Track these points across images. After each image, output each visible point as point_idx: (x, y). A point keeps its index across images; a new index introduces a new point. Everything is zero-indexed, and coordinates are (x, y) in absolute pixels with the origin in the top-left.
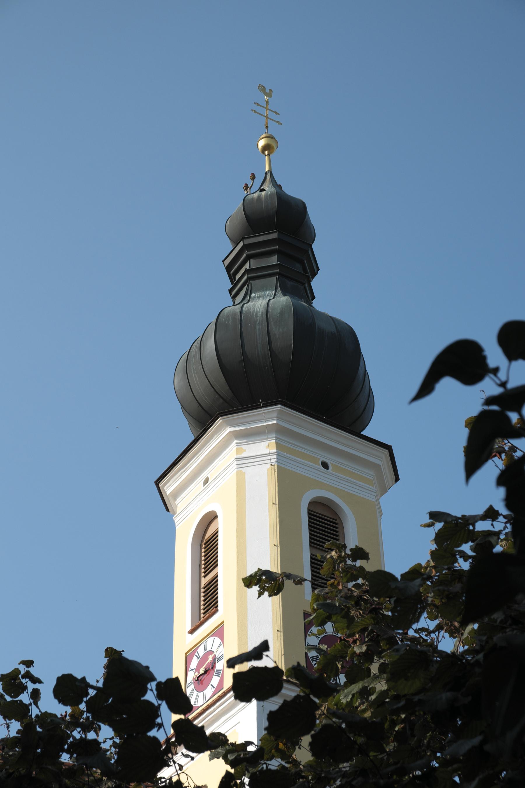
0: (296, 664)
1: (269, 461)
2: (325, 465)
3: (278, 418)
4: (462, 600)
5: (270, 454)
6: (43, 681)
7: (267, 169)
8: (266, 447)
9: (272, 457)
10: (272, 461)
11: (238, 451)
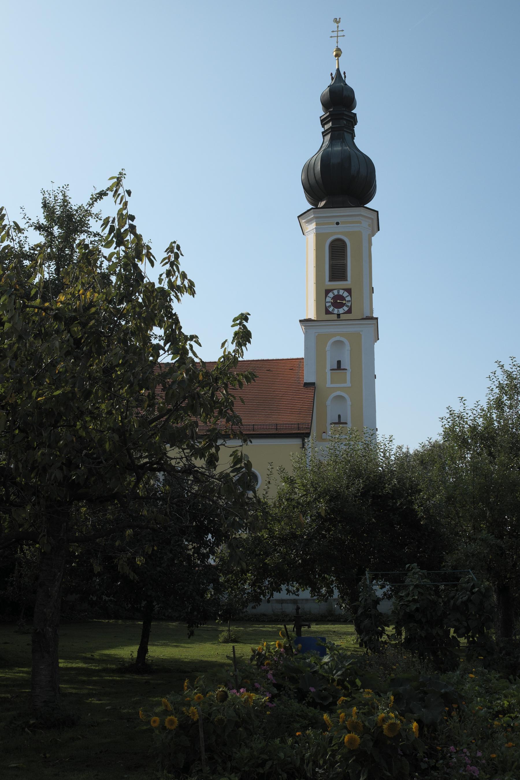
3: (314, 214)
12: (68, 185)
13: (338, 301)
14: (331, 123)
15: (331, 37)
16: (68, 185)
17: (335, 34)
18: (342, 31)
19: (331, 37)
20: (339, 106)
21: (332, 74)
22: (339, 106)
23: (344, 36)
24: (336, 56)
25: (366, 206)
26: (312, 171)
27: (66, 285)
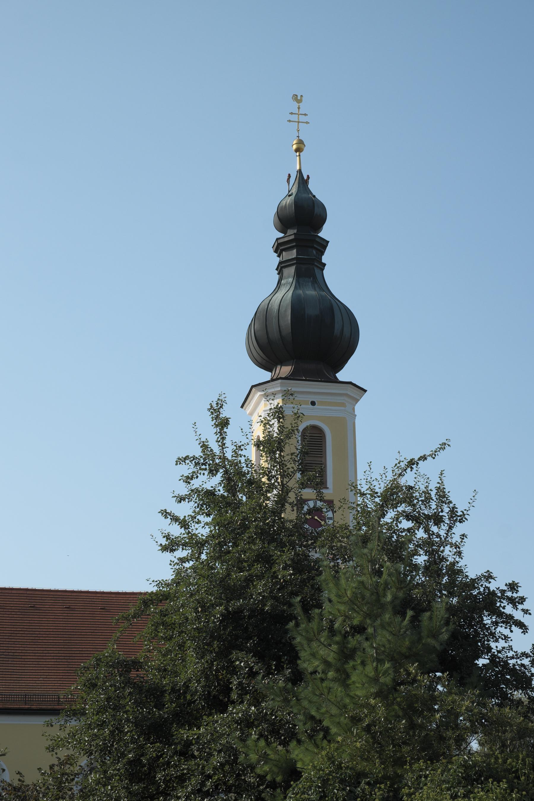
0: (516, 582)
2: (313, 403)
3: (281, 386)
6: (280, 193)
7: (298, 168)
12: (371, 462)
13: (316, 518)
15: (289, 121)
16: (371, 462)
17: (294, 118)
18: (305, 115)
19: (289, 121)
20: (302, 227)
22: (302, 227)
24: (297, 150)
25: (341, 376)
26: (275, 321)
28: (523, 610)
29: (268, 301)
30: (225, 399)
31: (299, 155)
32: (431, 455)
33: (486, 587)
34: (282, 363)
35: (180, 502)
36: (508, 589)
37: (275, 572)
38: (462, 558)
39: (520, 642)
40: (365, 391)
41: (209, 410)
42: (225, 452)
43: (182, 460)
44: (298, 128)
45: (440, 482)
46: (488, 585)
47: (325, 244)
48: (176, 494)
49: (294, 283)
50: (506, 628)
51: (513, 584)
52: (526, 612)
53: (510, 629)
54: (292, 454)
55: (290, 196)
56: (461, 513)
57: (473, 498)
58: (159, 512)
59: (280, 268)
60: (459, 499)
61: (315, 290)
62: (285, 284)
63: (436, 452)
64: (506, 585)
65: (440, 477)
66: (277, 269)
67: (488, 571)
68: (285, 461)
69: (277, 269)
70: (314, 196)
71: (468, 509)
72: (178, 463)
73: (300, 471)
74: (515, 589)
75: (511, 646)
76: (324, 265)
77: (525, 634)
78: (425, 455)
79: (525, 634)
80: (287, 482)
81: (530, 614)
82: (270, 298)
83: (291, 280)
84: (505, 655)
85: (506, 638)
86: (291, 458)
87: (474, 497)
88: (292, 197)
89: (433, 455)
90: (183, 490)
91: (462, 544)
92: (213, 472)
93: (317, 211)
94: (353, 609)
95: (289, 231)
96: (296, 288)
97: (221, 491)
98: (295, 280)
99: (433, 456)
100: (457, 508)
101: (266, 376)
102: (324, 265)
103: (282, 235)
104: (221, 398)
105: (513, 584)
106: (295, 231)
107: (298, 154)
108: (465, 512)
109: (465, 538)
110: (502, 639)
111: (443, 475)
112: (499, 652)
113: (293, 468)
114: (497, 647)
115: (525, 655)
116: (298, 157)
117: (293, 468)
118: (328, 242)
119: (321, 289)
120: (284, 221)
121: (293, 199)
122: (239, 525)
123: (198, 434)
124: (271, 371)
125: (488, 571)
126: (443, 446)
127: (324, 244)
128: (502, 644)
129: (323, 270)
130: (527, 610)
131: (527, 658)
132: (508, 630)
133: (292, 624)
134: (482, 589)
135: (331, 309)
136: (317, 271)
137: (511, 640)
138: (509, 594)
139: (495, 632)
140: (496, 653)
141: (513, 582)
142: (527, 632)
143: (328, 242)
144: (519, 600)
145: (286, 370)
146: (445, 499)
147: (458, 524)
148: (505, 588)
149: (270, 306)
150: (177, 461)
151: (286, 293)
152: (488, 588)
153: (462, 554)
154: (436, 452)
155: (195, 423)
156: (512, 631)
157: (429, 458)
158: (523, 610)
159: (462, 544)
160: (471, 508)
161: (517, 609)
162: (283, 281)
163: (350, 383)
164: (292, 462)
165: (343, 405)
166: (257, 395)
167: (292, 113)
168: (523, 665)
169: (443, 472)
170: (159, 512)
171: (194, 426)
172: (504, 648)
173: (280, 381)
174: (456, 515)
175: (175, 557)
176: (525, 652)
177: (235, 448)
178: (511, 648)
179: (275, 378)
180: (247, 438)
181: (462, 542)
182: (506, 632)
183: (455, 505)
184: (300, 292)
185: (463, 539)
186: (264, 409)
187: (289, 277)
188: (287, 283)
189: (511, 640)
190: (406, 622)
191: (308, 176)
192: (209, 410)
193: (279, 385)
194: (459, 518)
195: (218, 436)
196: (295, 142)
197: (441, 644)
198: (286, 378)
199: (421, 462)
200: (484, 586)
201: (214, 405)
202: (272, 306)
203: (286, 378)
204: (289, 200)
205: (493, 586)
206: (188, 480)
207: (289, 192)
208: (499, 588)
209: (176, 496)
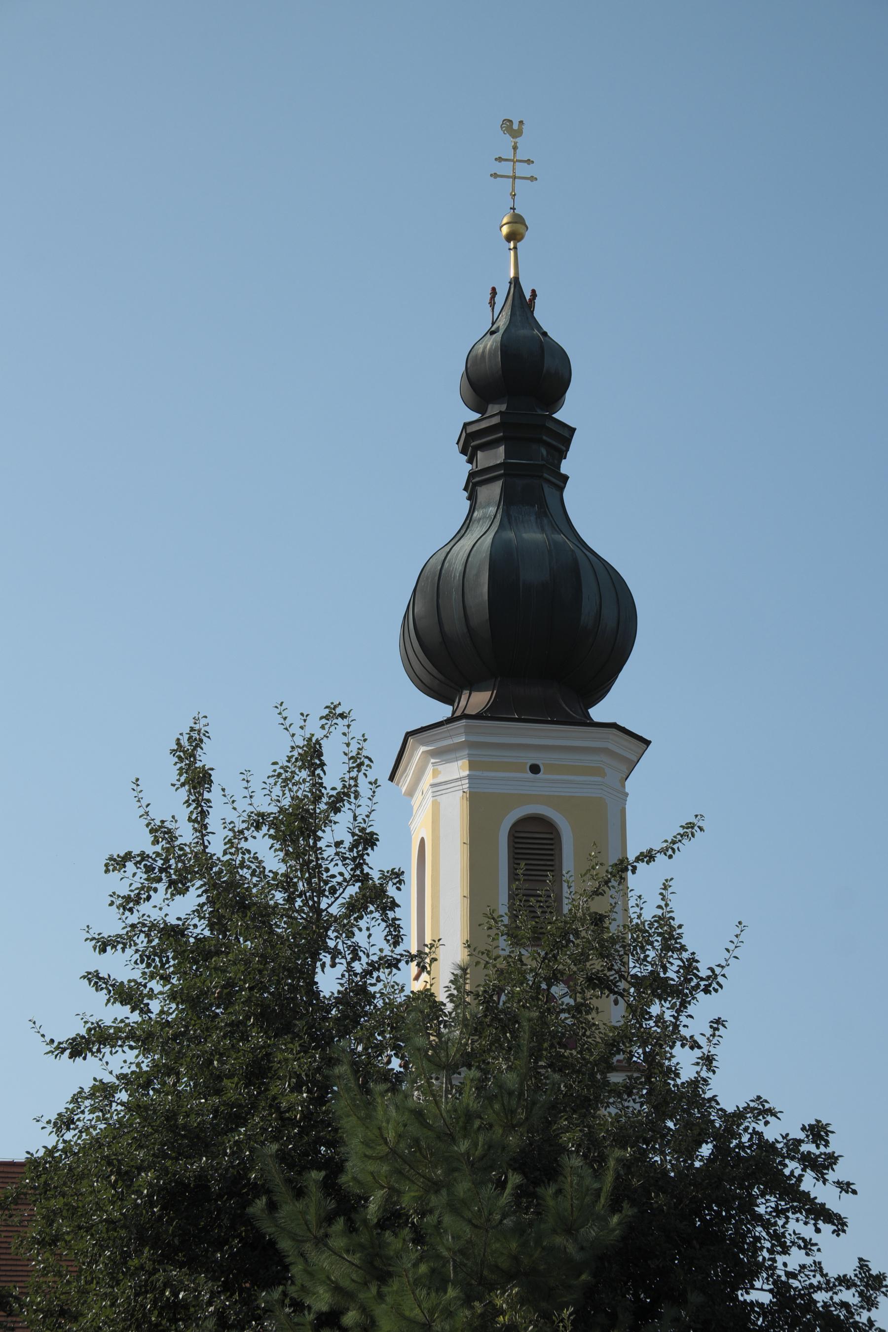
0: (824, 1123)
1: (461, 787)
2: (535, 769)
3: (467, 733)
4: (677, 1259)
5: (460, 779)
6: (472, 327)
7: (512, 275)
8: (457, 769)
9: (463, 782)
10: (464, 787)
11: (435, 773)
14: (502, 449)
15: (495, 175)
17: (506, 168)
18: (529, 162)
19: (495, 175)
20: (519, 398)
21: (494, 292)
22: (519, 398)
23: (532, 179)
24: (510, 237)
25: (598, 713)
26: (456, 596)
27: (262, 1059)
28: (838, 1184)
29: (444, 555)
30: (206, 728)
31: (515, 248)
32: (664, 851)
33: (755, 1132)
34: (473, 685)
35: (104, 951)
36: (807, 1136)
37: (274, 1098)
38: (714, 1072)
39: (837, 1255)
40: (647, 743)
41: (173, 752)
42: (206, 843)
43: (118, 863)
44: (513, 190)
45: (663, 904)
46: (760, 1127)
47: (566, 434)
48: (94, 933)
49: (499, 516)
50: (806, 1223)
51: (818, 1126)
52: (845, 1187)
53: (815, 1225)
54: (338, 844)
55: (492, 333)
56: (710, 973)
57: (735, 940)
58: (84, 977)
59: (472, 486)
60: (703, 943)
61: (543, 530)
62: (480, 519)
63: (674, 842)
64: (803, 1129)
65: (661, 894)
66: (465, 489)
67: (759, 1098)
68: (323, 858)
69: (465, 489)
70: (545, 334)
71: (724, 963)
72: (111, 868)
73: (357, 881)
74: (822, 1138)
75: (820, 1263)
76: (565, 478)
77: (838, 1235)
78: (651, 850)
79: (838, 1235)
80: (330, 906)
81: (854, 1192)
82: (447, 549)
83: (492, 510)
84: (807, 1283)
85: (807, 1246)
86: (337, 854)
87: (737, 936)
88: (498, 336)
89: (669, 850)
90: (113, 924)
91: (715, 1041)
92: (178, 887)
93: (549, 363)
94: (400, 1172)
95: (490, 406)
96: (501, 526)
97: (201, 929)
98: (500, 511)
99: (670, 852)
100: (697, 961)
101: (442, 711)
102: (565, 478)
103: (476, 416)
104: (197, 727)
105: (818, 1126)
106: (503, 407)
107: (512, 245)
108: (718, 970)
109: (721, 1027)
110: (799, 1247)
111: (670, 890)
112: (791, 1275)
113: (341, 874)
114: (785, 1265)
115: (844, 1281)
116: (512, 252)
117: (341, 874)
118: (574, 429)
119: (558, 530)
120: (480, 387)
121: (499, 339)
122: (218, 997)
123: (144, 803)
124: (452, 704)
125: (759, 1098)
126: (690, 829)
127: (564, 436)
128: (795, 1259)
129: (561, 489)
130: (848, 1184)
131: (848, 1288)
132: (811, 1227)
133: (261, 1202)
134: (745, 1138)
135: (575, 571)
136: (548, 490)
137: (819, 1250)
138: (807, 1147)
139: (783, 1233)
140: (784, 1278)
141: (818, 1121)
142: (844, 1231)
143: (572, 430)
144: (825, 1160)
145: (478, 700)
146: (673, 942)
147: (700, 995)
148: (801, 1135)
149: (446, 565)
150: (107, 865)
151: (482, 539)
152: (760, 1135)
153: (714, 1063)
154: (674, 842)
155: (137, 780)
156: (818, 1231)
157: (660, 858)
158: (838, 1184)
159: (715, 1041)
160: (732, 961)
161: (825, 1181)
162: (475, 514)
163: (614, 726)
164: (340, 863)
165: (598, 771)
166: (418, 752)
167: (499, 159)
168: (845, 1305)
169: (670, 883)
170: (84, 977)
171: (134, 786)
172: (803, 1267)
173: (463, 722)
174: (697, 976)
175: (111, 1073)
176: (845, 1276)
177: (231, 834)
178: (818, 1267)
179: (458, 713)
180: (235, 809)
181: (713, 1035)
182: (807, 1232)
183: (693, 953)
184: (510, 535)
185: (717, 1029)
186: (432, 781)
187: (488, 505)
188: (484, 517)
189: (819, 1250)
190: (506, 1197)
191: (534, 291)
192: (173, 752)
193: (462, 730)
194: (702, 983)
195: (192, 808)
196: (505, 220)
197: (582, 1248)
198: (478, 716)
199: (640, 866)
200: (750, 1131)
201: (185, 742)
202: (450, 566)
203: (478, 716)
204: (492, 342)
205: (772, 1132)
206: (129, 903)
207: (493, 324)
208: (787, 1135)
209: (93, 939)
